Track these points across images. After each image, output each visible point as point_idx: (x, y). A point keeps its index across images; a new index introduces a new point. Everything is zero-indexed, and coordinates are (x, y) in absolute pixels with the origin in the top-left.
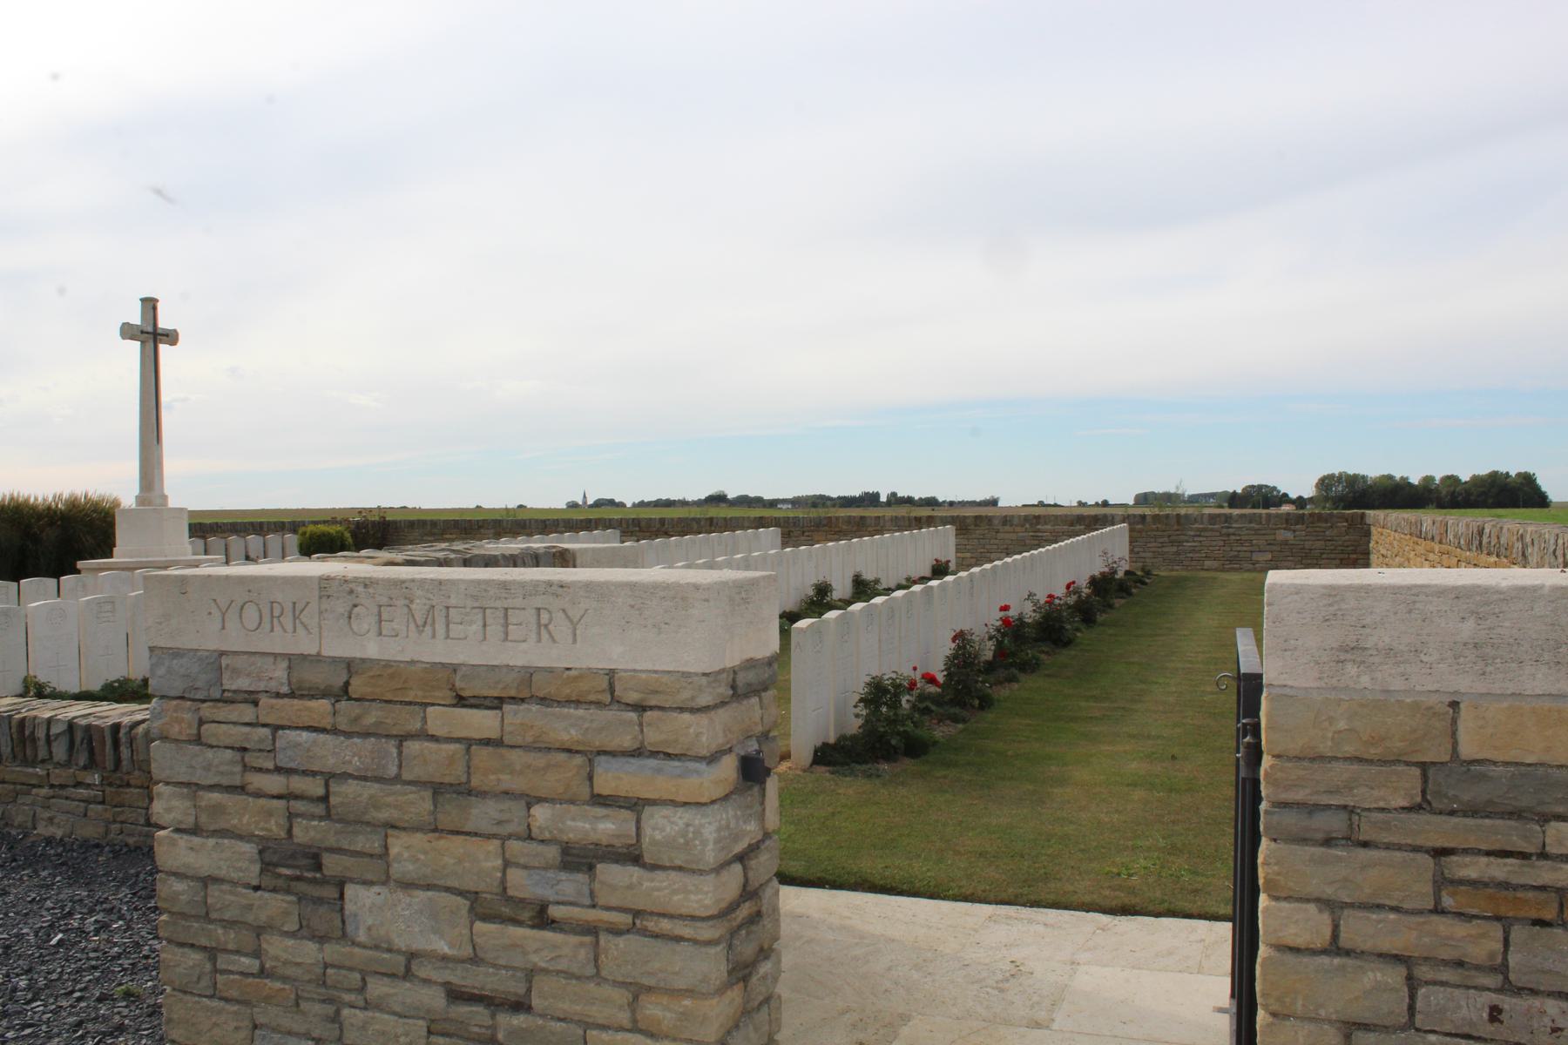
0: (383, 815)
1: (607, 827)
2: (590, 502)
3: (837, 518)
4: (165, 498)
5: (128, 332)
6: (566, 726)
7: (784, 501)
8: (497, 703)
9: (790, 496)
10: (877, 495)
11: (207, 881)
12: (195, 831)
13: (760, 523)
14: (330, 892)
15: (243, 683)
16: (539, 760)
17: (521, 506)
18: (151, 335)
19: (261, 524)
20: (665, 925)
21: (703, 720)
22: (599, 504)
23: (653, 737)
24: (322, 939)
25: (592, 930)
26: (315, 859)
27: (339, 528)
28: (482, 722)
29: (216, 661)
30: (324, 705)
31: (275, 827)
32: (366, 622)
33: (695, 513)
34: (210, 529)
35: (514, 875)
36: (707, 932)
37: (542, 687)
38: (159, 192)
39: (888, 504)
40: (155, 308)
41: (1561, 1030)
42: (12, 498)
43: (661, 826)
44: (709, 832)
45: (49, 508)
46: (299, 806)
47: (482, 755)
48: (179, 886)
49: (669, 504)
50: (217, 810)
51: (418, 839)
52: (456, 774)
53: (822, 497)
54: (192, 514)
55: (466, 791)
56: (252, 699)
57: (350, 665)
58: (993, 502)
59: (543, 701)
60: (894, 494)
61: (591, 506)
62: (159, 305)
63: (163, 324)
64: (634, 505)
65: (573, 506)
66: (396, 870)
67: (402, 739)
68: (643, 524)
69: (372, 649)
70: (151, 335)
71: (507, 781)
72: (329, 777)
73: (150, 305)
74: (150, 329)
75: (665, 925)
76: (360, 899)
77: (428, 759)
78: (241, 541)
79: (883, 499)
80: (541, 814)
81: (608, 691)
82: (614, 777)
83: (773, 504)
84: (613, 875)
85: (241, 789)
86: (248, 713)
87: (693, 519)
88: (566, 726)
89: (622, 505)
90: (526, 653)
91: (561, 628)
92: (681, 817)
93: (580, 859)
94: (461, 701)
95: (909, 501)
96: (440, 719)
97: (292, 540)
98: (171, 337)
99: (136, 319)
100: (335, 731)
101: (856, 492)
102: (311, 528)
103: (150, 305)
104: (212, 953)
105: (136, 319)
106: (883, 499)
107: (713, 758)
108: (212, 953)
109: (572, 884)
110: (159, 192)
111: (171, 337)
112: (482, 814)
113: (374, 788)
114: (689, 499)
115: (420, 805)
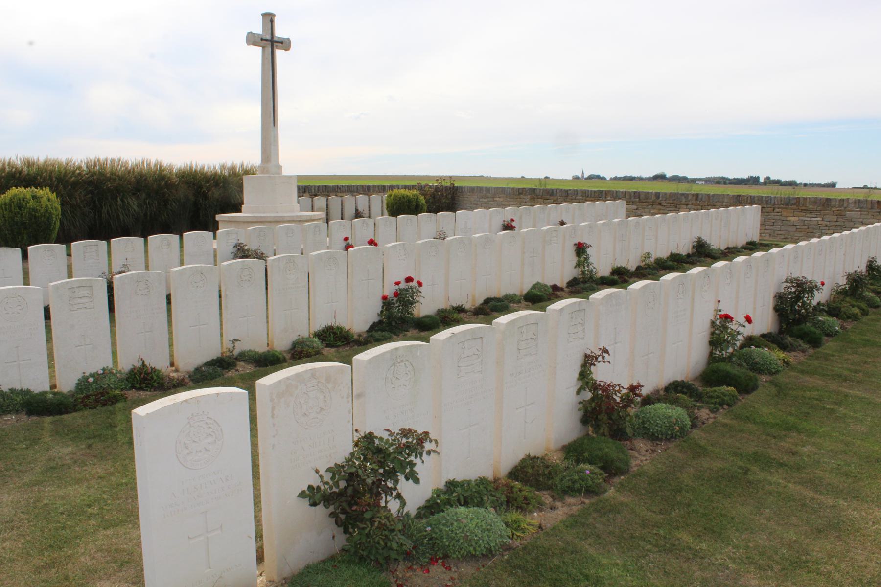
2: (586, 176)
3: (805, 199)
4: (280, 167)
7: (700, 180)
9: (703, 177)
10: (757, 179)
13: (739, 201)
17: (546, 177)
18: (270, 43)
19: (369, 187)
22: (591, 177)
27: (415, 192)
33: (695, 189)
34: (311, 190)
38: (47, 310)
39: (765, 183)
40: (272, 21)
41: (376, 245)
42: (191, 168)
45: (216, 174)
49: (632, 179)
53: (723, 178)
54: (300, 178)
58: (833, 185)
60: (768, 178)
61: (586, 179)
62: (276, 20)
63: (279, 33)
64: (611, 179)
65: (576, 178)
68: (642, 196)
70: (270, 43)
73: (269, 19)
74: (268, 37)
78: (339, 199)
79: (762, 180)
83: (694, 181)
87: (683, 194)
89: (604, 178)
95: (778, 182)
97: (378, 201)
98: (285, 44)
99: (258, 29)
101: (745, 175)
102: (396, 191)
103: (269, 19)
105: (258, 29)
106: (762, 180)
110: (47, 310)
111: (285, 44)
114: (644, 176)
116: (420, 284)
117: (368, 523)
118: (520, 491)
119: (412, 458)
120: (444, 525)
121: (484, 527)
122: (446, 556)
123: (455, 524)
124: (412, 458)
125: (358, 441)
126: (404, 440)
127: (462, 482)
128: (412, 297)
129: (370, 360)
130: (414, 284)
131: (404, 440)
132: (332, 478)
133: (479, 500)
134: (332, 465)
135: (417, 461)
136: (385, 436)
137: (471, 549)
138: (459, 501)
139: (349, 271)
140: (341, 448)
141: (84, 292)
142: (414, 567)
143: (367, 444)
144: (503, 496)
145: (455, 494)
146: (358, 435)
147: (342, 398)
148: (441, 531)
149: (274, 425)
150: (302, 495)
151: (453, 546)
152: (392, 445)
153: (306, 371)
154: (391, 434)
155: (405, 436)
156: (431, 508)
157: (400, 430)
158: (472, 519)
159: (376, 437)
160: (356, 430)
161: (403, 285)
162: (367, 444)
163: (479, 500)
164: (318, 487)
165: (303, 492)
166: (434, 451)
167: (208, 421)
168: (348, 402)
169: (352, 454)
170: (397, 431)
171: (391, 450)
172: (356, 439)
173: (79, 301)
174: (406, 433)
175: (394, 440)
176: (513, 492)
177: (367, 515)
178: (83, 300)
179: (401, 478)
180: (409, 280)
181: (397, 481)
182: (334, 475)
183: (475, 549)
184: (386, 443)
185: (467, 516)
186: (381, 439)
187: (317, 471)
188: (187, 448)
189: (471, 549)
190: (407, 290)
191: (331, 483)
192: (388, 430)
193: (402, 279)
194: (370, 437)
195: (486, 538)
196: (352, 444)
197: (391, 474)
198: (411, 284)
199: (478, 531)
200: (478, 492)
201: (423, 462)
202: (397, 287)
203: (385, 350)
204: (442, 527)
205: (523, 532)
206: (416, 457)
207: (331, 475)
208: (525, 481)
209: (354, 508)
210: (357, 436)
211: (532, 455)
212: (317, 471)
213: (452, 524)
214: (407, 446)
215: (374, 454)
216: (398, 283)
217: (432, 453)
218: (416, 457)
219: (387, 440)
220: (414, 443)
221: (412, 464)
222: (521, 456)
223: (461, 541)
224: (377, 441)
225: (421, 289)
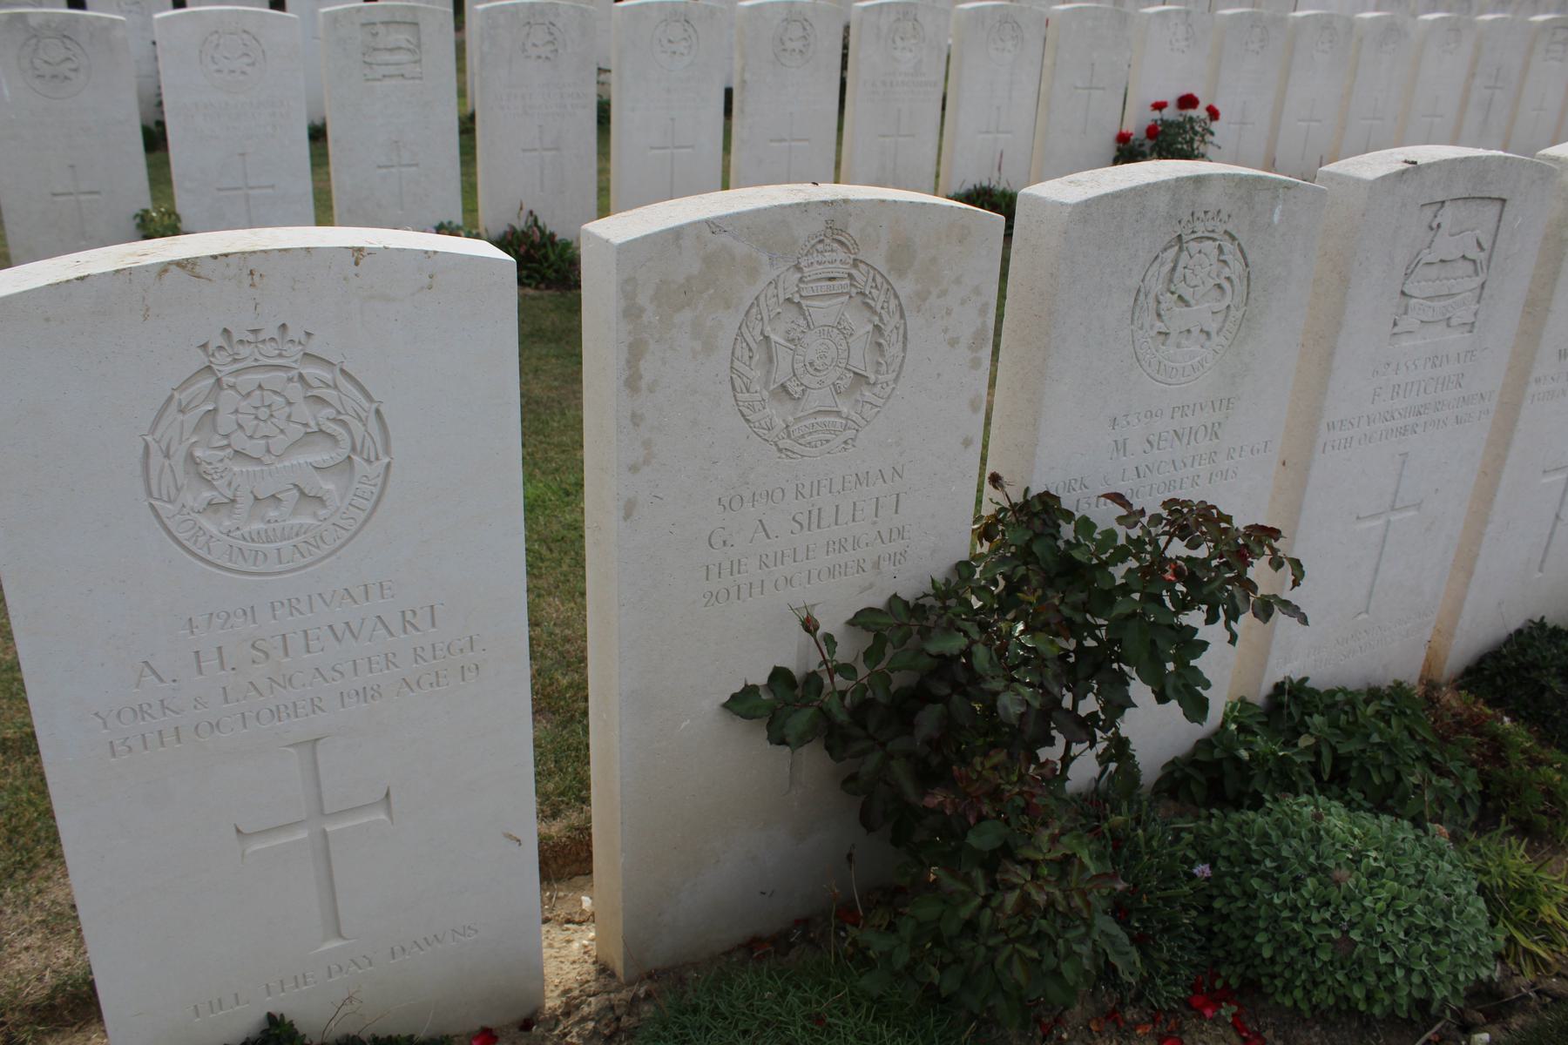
116: (1213, 113)
117: (978, 874)
118: (1535, 763)
119: (1195, 618)
120: (1264, 876)
121: (1420, 919)
122: (1251, 989)
123: (1311, 883)
124: (1195, 618)
125: (996, 519)
126: (1177, 549)
127: (1332, 693)
128: (1191, 141)
129: (1088, 204)
130: (1200, 112)
131: (1177, 549)
132: (871, 655)
133: (1388, 776)
134: (879, 601)
135: (1214, 634)
136: (1106, 516)
137: (1358, 992)
138: (1316, 771)
139: (1047, 62)
140: (931, 537)
141: (401, 37)
142: (1131, 1014)
143: (1032, 536)
144: (1472, 773)
145: (1305, 741)
146: (997, 495)
147: (953, 343)
148: (1251, 896)
149: (636, 419)
150: (742, 703)
151: (1289, 965)
152: (1121, 554)
153: (804, 208)
154: (1132, 516)
155: (1182, 530)
156: (1208, 777)
157: (1165, 504)
158: (1374, 874)
159: (1068, 515)
160: (995, 480)
161: (1171, 113)
162: (1032, 536)
163: (1388, 776)
164: (812, 678)
165: (750, 691)
166: (1287, 606)
167: (311, 371)
168: (976, 364)
169: (963, 569)
170: (1154, 507)
171: (1119, 572)
172: (988, 510)
173: (387, 57)
174: (1189, 519)
175: (1139, 543)
176: (1504, 764)
177: (983, 839)
178: (397, 57)
179: (1139, 691)
180: (1188, 101)
181: (1118, 704)
182: (880, 641)
183: (1370, 998)
184: (1102, 546)
185: (1359, 857)
186: (1086, 525)
187: (809, 625)
188: (205, 480)
189: (1358, 992)
190: (1180, 125)
191: (863, 671)
192: (1117, 498)
193: (1171, 95)
194: (1042, 511)
195: (1424, 965)
196: (967, 526)
197: (1099, 669)
198: (1191, 113)
199: (1391, 929)
200: (1389, 747)
201: (1233, 639)
202: (1156, 115)
203: (1151, 179)
204: (1256, 883)
205: (1549, 941)
206: (1211, 619)
207: (867, 640)
208: (1534, 713)
209: (935, 799)
210: (993, 500)
211: (1550, 622)
212: (809, 625)
213: (1297, 883)
214: (1191, 573)
215: (1049, 582)
216: (1159, 106)
217: (1279, 617)
218: (1211, 619)
219: (1110, 535)
220: (1223, 561)
221: (1191, 645)
222: (1515, 622)
223: (1325, 956)
224: (1068, 531)
225: (1214, 126)
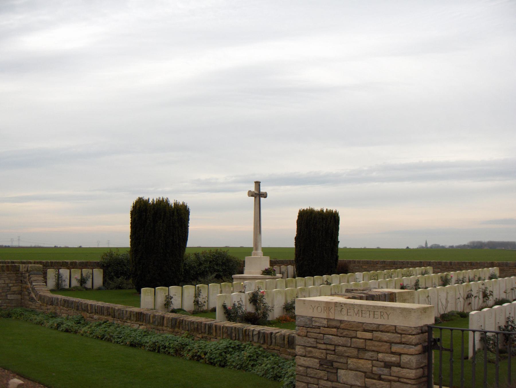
0: (347, 354)
1: (394, 359)
5: (251, 194)
6: (385, 336)
8: (372, 331)
11: (308, 367)
12: (304, 356)
14: (335, 371)
15: (317, 324)
16: (380, 344)
18: (258, 195)
20: (405, 380)
21: (414, 337)
23: (403, 340)
24: (332, 381)
25: (390, 381)
26: (331, 362)
28: (368, 335)
29: (311, 319)
30: (335, 330)
31: (323, 356)
32: (344, 311)
35: (374, 368)
36: (413, 382)
37: (381, 328)
43: (405, 359)
44: (414, 361)
46: (328, 352)
47: (368, 342)
48: (301, 368)
50: (310, 352)
51: (355, 360)
52: (362, 346)
55: (364, 350)
56: (319, 327)
57: (341, 321)
59: (382, 331)
66: (349, 366)
67: (352, 338)
69: (345, 318)
71: (374, 348)
72: (335, 345)
75: (405, 380)
76: (341, 372)
77: (360, 343)
80: (380, 355)
81: (395, 330)
82: (395, 348)
84: (395, 369)
85: (315, 347)
86: (318, 331)
88: (385, 336)
90: (379, 321)
91: (385, 316)
92: (409, 357)
93: (388, 365)
94: (365, 331)
96: (360, 334)
99: (253, 189)
100: (337, 336)
104: (308, 383)
105: (253, 189)
107: (416, 345)
108: (308, 383)
109: (386, 371)
112: (369, 355)
113: (345, 348)
115: (355, 352)
